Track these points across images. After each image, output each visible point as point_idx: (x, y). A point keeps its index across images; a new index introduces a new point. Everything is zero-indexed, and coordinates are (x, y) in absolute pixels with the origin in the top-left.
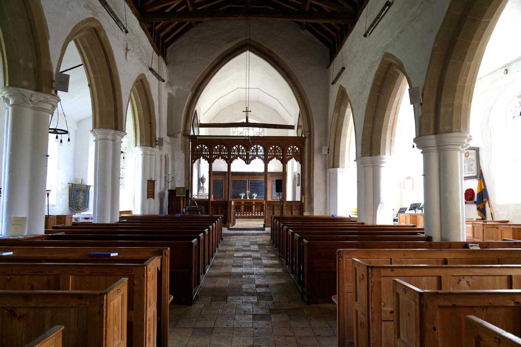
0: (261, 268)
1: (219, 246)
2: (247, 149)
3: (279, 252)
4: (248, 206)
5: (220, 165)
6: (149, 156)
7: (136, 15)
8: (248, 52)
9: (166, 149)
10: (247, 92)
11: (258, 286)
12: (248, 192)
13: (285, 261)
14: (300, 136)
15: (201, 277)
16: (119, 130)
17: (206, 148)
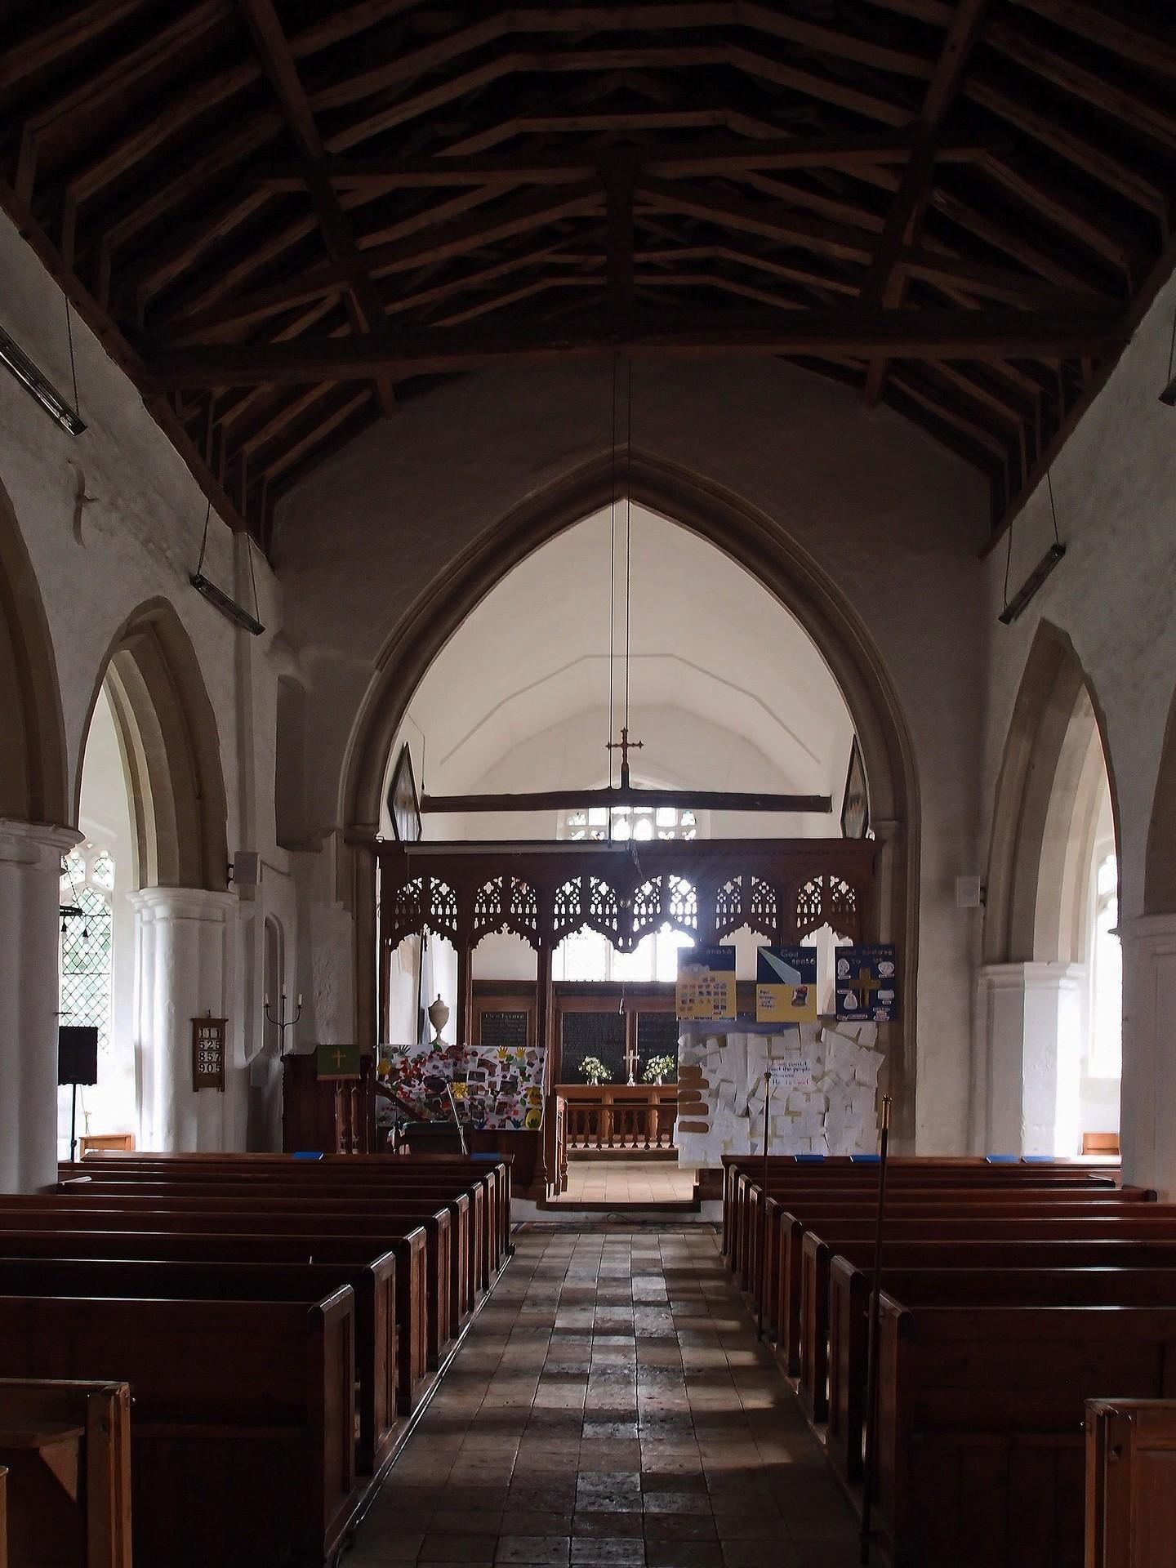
0: (674, 1385)
1: (494, 1281)
2: (624, 888)
3: (758, 1311)
4: (629, 1114)
5: (505, 956)
7: (124, 362)
8: (625, 501)
9: (272, 895)
10: (630, 677)
11: (654, 1482)
13: (786, 1356)
14: (858, 835)
15: (383, 1437)
16: (49, 823)
17: (444, 889)
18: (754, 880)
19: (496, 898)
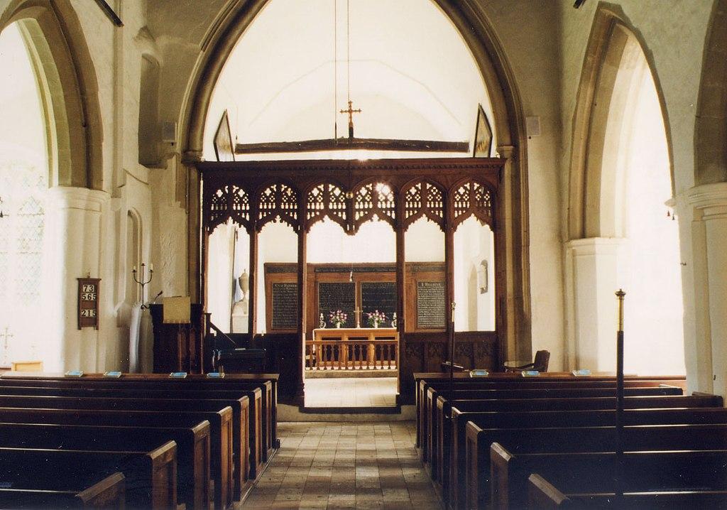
4: (385, 346)
6: (82, 213)
9: (135, 196)
12: (358, 311)
17: (241, 193)
18: (428, 186)
19: (272, 199)
